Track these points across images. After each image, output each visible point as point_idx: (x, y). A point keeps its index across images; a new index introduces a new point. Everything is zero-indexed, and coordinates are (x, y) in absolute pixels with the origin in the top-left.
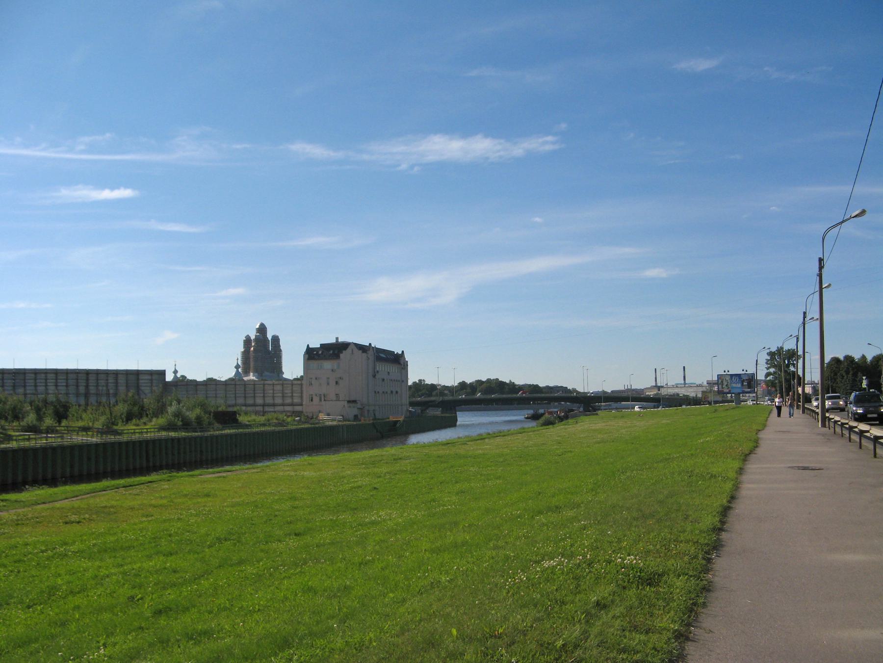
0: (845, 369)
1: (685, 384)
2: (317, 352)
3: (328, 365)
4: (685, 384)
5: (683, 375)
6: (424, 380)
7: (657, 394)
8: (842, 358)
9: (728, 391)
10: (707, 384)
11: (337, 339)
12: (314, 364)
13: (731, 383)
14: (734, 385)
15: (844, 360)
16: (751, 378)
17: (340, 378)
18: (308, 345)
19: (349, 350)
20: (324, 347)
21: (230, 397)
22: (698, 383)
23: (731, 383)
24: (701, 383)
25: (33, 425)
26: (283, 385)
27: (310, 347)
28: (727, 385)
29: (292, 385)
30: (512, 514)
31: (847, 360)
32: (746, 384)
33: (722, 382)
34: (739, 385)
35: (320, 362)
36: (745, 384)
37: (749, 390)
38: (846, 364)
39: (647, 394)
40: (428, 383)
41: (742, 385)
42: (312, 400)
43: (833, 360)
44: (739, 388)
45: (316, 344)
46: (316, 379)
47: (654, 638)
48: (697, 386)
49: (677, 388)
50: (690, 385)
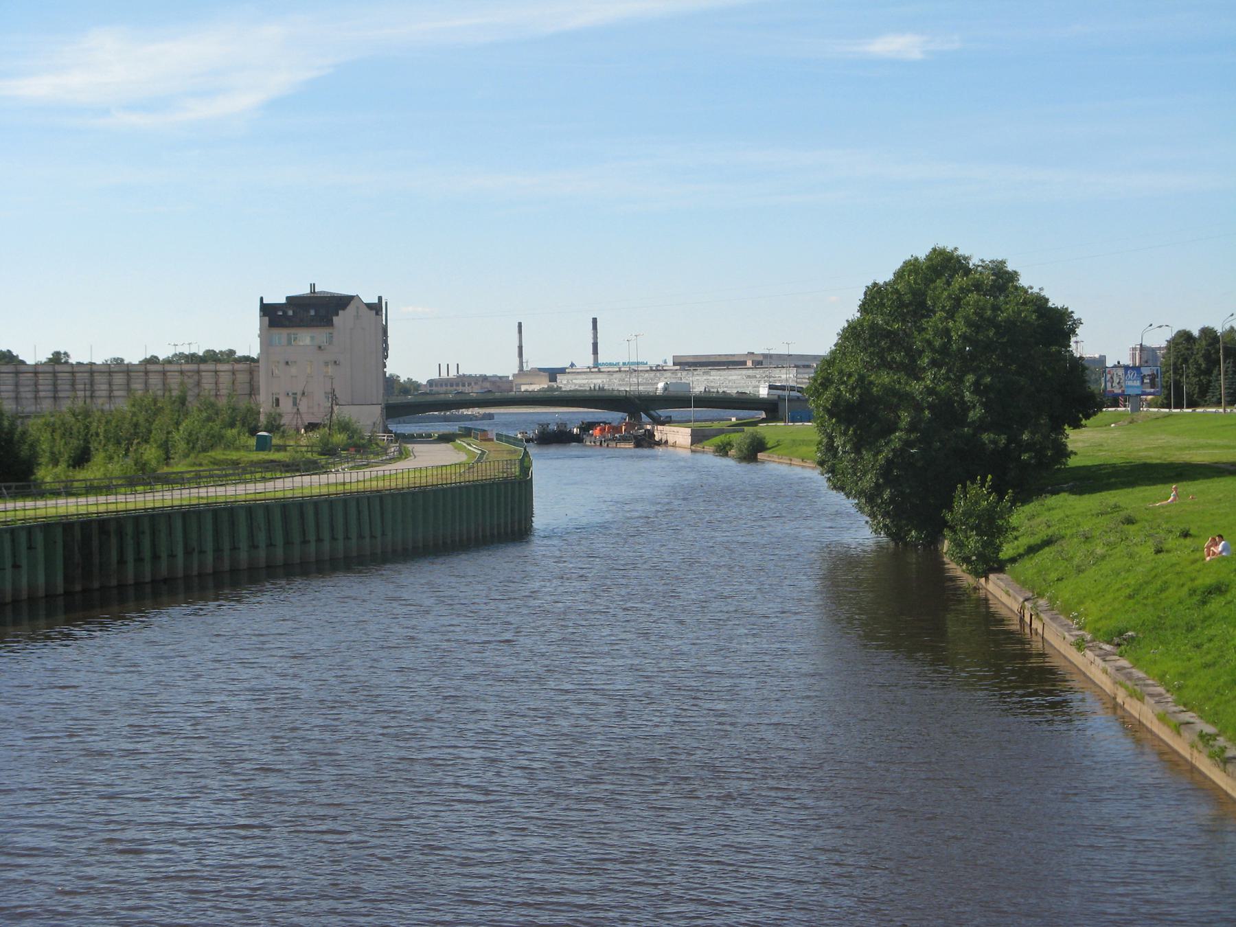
0: (1203, 352)
1: (596, 364)
2: (285, 313)
3: (306, 338)
4: (596, 364)
5: (592, 341)
6: (65, 353)
7: (550, 389)
8: (1196, 333)
9: (1120, 391)
10: (675, 364)
11: (313, 286)
12: (281, 334)
13: (1125, 380)
14: (1130, 383)
15: (1200, 338)
16: (1155, 372)
17: (335, 362)
18: (262, 299)
19: (351, 309)
20: (294, 302)
21: (26, 398)
22: (654, 361)
23: (1125, 380)
24: (661, 363)
25: (560, 431)
26: (17, 373)
27: (264, 302)
28: (1119, 383)
29: (146, 373)
30: (923, 539)
31: (1205, 336)
32: (1148, 381)
33: (1112, 378)
34: (1138, 383)
35: (293, 331)
36: (1145, 381)
37: (1152, 390)
38: (1204, 343)
39: (523, 388)
40: (467, 373)
41: (1142, 382)
42: (278, 405)
43: (1181, 336)
44: (1137, 387)
45: (277, 297)
46: (287, 363)
47: (803, 717)
48: (651, 370)
49: (600, 375)
50: (633, 367)
